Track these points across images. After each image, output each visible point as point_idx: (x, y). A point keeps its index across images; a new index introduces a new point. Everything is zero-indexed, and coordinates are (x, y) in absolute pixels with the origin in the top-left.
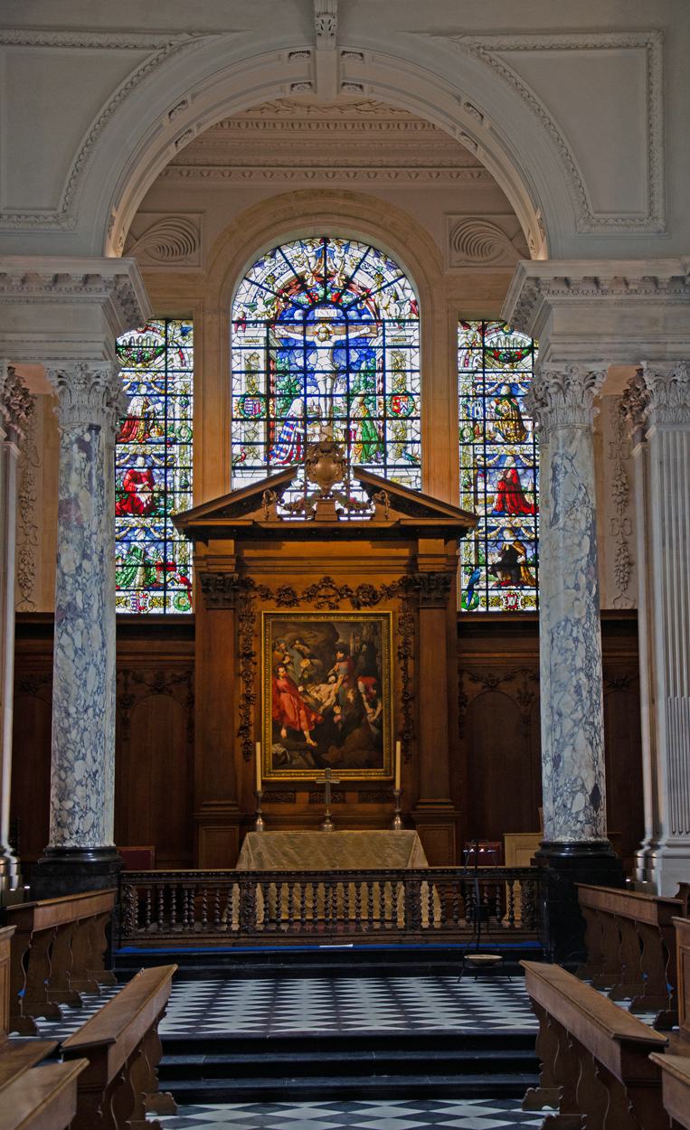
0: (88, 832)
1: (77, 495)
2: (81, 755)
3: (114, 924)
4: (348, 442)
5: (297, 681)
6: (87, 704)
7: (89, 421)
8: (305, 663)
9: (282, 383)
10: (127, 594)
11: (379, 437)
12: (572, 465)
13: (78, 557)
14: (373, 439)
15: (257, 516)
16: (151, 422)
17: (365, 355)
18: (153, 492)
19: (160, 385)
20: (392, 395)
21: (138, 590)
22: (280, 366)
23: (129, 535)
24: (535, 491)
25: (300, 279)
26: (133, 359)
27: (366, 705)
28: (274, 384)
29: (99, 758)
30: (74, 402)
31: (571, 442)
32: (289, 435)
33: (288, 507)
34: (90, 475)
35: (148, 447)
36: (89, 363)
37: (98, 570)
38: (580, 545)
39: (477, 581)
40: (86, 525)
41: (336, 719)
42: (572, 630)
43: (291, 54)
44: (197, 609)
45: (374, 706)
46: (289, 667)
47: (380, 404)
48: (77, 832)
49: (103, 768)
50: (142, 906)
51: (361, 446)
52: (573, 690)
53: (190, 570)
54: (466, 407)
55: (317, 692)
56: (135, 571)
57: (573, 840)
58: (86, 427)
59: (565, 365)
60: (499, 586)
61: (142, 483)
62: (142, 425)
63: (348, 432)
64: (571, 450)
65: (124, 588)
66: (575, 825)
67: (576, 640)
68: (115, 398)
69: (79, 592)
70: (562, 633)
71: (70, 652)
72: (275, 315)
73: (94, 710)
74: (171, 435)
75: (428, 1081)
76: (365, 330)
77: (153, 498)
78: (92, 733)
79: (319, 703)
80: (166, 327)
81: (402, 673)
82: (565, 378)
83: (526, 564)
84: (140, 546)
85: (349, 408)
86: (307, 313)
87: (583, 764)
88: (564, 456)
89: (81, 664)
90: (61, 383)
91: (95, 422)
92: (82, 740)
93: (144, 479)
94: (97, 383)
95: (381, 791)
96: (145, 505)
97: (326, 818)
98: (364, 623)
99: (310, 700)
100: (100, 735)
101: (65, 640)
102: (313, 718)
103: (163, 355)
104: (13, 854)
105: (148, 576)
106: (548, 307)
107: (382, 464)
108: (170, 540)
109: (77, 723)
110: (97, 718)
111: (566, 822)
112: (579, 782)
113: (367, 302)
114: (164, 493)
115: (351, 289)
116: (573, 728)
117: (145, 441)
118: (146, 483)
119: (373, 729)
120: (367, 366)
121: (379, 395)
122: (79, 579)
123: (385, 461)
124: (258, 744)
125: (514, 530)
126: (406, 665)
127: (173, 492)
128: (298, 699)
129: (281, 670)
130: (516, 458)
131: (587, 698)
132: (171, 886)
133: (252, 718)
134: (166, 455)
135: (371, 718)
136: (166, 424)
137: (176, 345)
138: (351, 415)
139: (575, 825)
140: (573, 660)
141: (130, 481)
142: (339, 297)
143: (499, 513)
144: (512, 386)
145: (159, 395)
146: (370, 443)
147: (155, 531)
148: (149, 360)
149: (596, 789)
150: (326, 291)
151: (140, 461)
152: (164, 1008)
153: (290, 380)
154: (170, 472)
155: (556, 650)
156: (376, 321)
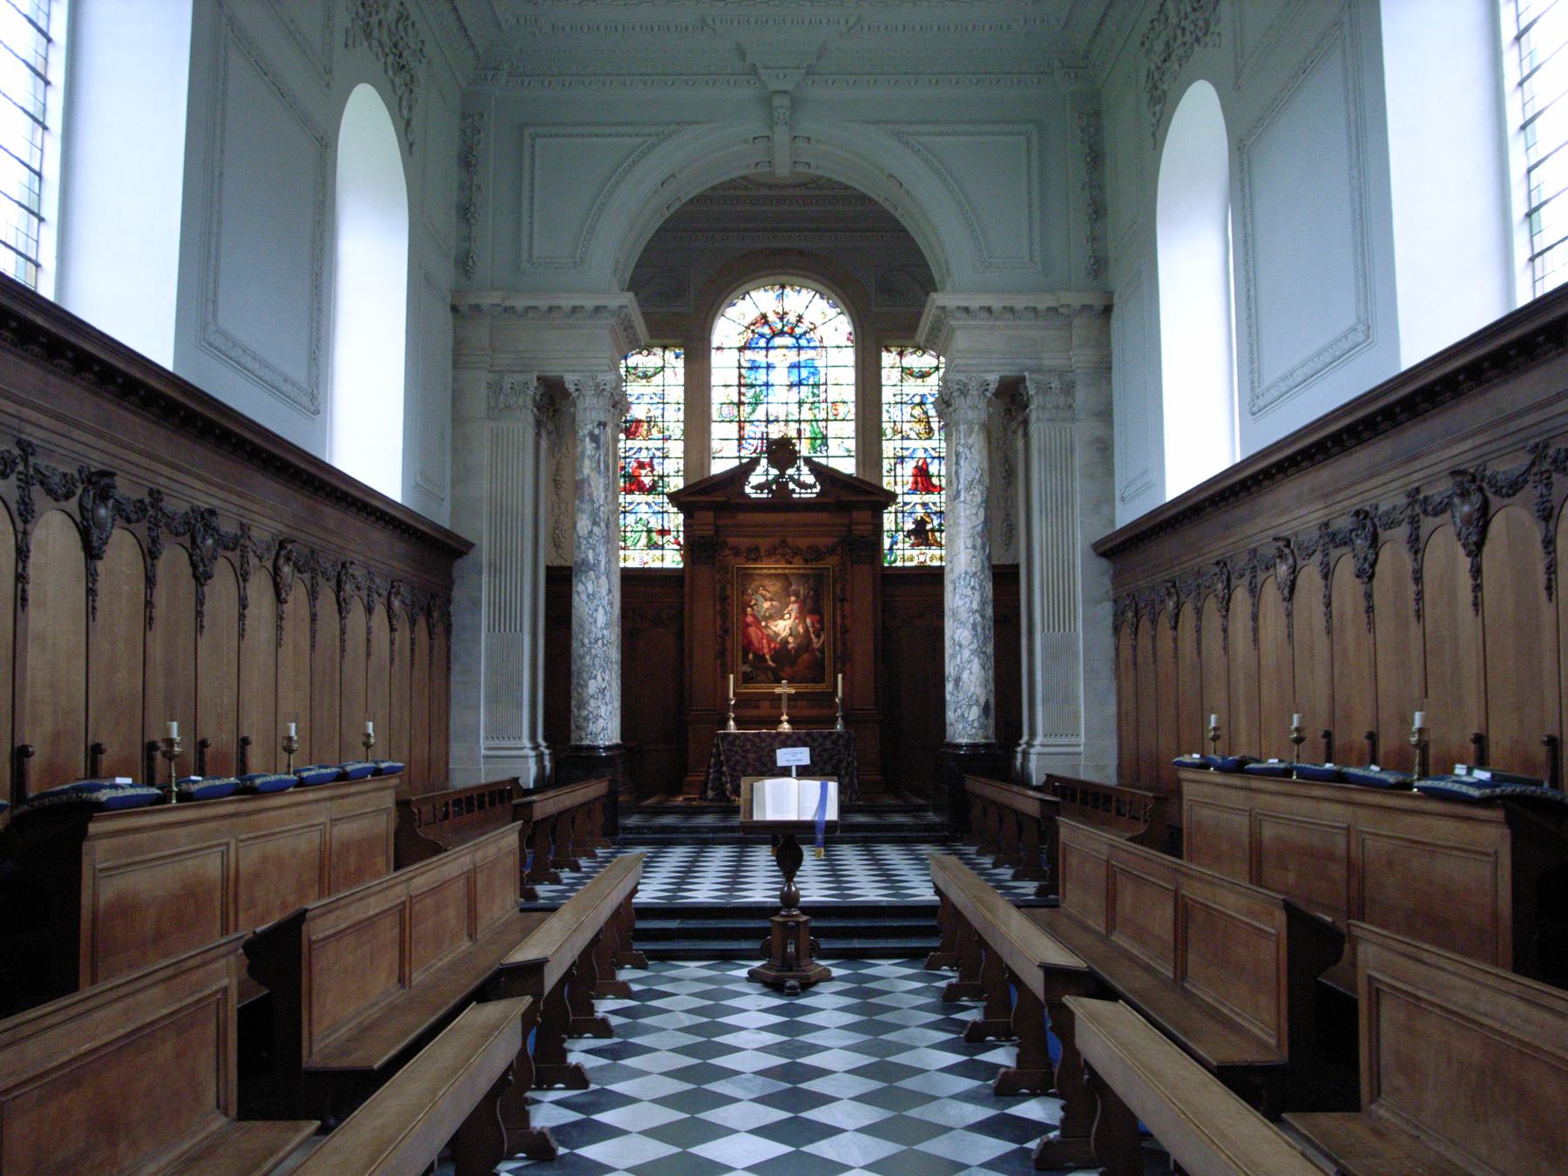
1: (588, 476)
3: (610, 806)
4: (799, 438)
5: (760, 617)
7: (598, 419)
9: (750, 393)
13: (589, 523)
20: (833, 403)
24: (939, 476)
26: (639, 377)
27: (813, 636)
29: (607, 678)
30: (587, 405)
33: (753, 488)
34: (599, 459)
36: (598, 374)
37: (605, 534)
39: (896, 543)
40: (595, 499)
41: (790, 646)
43: (755, 138)
44: (685, 564)
45: (818, 636)
46: (755, 607)
49: (610, 686)
51: (809, 441)
53: (681, 534)
54: (888, 411)
57: (969, 741)
58: (595, 424)
60: (913, 546)
62: (646, 425)
63: (799, 431)
64: (971, 441)
68: (620, 403)
69: (591, 551)
70: (962, 583)
71: (584, 597)
74: (667, 433)
75: (857, 944)
76: (811, 354)
79: (777, 635)
82: (965, 385)
83: (933, 530)
84: (645, 517)
86: (768, 341)
88: (965, 445)
89: (592, 606)
90: (577, 390)
91: (603, 420)
92: (594, 664)
94: (604, 390)
99: (771, 632)
101: (580, 588)
102: (773, 645)
104: (547, 747)
105: (650, 539)
106: (953, 330)
107: (825, 454)
108: (666, 512)
111: (964, 728)
112: (974, 697)
114: (662, 477)
117: (648, 438)
119: (818, 654)
125: (924, 505)
127: (668, 476)
129: (749, 609)
130: (926, 450)
134: (663, 449)
135: (816, 646)
140: (971, 603)
143: (914, 490)
144: (923, 396)
146: (815, 439)
148: (651, 377)
149: (987, 702)
151: (644, 453)
152: (636, 887)
154: (666, 461)
155: (958, 596)
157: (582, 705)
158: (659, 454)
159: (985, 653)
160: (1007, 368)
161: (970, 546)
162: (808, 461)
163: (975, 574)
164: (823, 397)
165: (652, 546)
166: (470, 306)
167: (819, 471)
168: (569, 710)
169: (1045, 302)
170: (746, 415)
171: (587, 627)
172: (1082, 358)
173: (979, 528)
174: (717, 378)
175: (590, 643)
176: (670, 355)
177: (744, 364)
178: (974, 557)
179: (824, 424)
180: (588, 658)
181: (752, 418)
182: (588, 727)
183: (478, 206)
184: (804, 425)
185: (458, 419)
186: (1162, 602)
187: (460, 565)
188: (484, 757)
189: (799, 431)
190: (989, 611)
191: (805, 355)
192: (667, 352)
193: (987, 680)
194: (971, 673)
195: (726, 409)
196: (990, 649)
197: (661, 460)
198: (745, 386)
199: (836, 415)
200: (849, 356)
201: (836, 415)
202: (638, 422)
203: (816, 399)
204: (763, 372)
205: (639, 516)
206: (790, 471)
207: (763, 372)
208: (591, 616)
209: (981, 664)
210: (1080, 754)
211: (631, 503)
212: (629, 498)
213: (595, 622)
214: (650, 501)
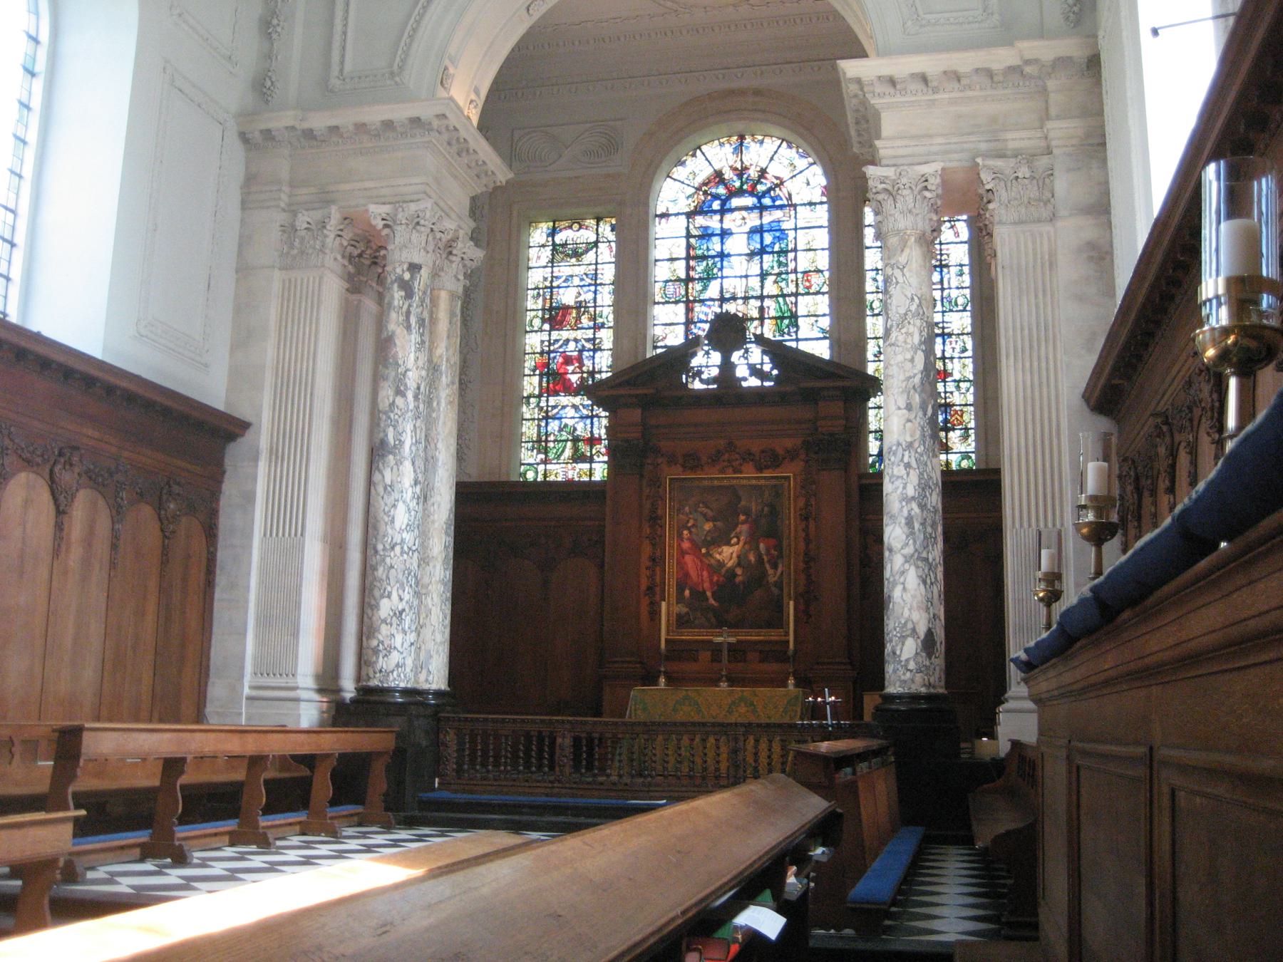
0: (392, 672)
2: (387, 593)
6: (394, 541)
7: (409, 260)
8: (708, 526)
9: (701, 267)
10: (558, 466)
11: (791, 312)
12: (904, 275)
13: (391, 393)
14: (786, 315)
16: (583, 309)
17: (778, 237)
18: (583, 372)
19: (590, 276)
20: (805, 273)
21: (567, 463)
22: (699, 252)
23: (561, 412)
25: (719, 175)
27: (768, 566)
28: (693, 269)
29: (406, 597)
31: (902, 251)
32: (706, 315)
35: (579, 332)
38: (912, 360)
40: (400, 362)
42: (903, 455)
45: (775, 567)
47: (792, 281)
48: (381, 671)
50: (460, 750)
51: (774, 322)
52: (903, 521)
54: (875, 280)
55: (720, 554)
56: (565, 446)
58: (405, 266)
59: (893, 169)
61: (573, 365)
63: (761, 309)
65: (555, 461)
66: (904, 674)
67: (908, 466)
69: (391, 429)
72: (696, 207)
73: (402, 548)
74: (599, 320)
76: (778, 214)
77: (582, 377)
78: (399, 571)
79: (721, 564)
80: (598, 225)
81: (804, 535)
82: (894, 183)
84: (570, 422)
85: (762, 287)
86: (724, 203)
87: (915, 605)
92: (388, 578)
93: (574, 361)
95: (775, 653)
96: (575, 385)
97: (722, 676)
98: (765, 486)
99: (713, 561)
100: (409, 574)
102: (715, 578)
103: (595, 249)
105: (576, 449)
109: (384, 560)
110: (405, 556)
112: (910, 626)
113: (780, 189)
115: (766, 178)
116: (903, 565)
118: (577, 365)
119: (775, 591)
120: (780, 247)
121: (791, 272)
122: (392, 415)
123: (797, 335)
124: (664, 605)
126: (807, 527)
128: (701, 561)
129: (685, 532)
131: (919, 530)
132: (532, 733)
133: (658, 580)
134: (594, 339)
136: (595, 311)
137: (605, 240)
138: (765, 293)
139: (904, 674)
140: (904, 488)
141: (562, 364)
142: (754, 187)
145: (590, 285)
146: (782, 318)
147: (584, 408)
148: (582, 254)
149: (930, 633)
150: (742, 182)
151: (572, 345)
153: (708, 264)
154: (598, 354)
156: (789, 205)
158: (589, 346)
159: (926, 560)
160: (956, 156)
161: (902, 405)
162: (760, 340)
163: (910, 445)
164: (791, 266)
165: (578, 458)
166: (261, 131)
169: (1002, 58)
170: (695, 294)
171: (382, 528)
173: (917, 380)
174: (660, 250)
175: (384, 549)
177: (694, 232)
178: (909, 421)
179: (793, 299)
180: (381, 569)
181: (704, 296)
182: (376, 662)
183: (282, 18)
184: (767, 303)
187: (235, 453)
188: (250, 698)
189: (761, 309)
191: (768, 218)
192: (601, 224)
193: (930, 601)
194: (904, 589)
195: (671, 288)
196: (936, 553)
197: (591, 353)
198: (696, 258)
199: (808, 288)
200: (822, 215)
201: (808, 288)
202: (566, 309)
203: (783, 269)
204: (716, 240)
205: (564, 421)
207: (716, 240)
208: (387, 514)
209: (920, 577)
211: (554, 407)
212: (552, 401)
213: (393, 521)
214: (578, 404)
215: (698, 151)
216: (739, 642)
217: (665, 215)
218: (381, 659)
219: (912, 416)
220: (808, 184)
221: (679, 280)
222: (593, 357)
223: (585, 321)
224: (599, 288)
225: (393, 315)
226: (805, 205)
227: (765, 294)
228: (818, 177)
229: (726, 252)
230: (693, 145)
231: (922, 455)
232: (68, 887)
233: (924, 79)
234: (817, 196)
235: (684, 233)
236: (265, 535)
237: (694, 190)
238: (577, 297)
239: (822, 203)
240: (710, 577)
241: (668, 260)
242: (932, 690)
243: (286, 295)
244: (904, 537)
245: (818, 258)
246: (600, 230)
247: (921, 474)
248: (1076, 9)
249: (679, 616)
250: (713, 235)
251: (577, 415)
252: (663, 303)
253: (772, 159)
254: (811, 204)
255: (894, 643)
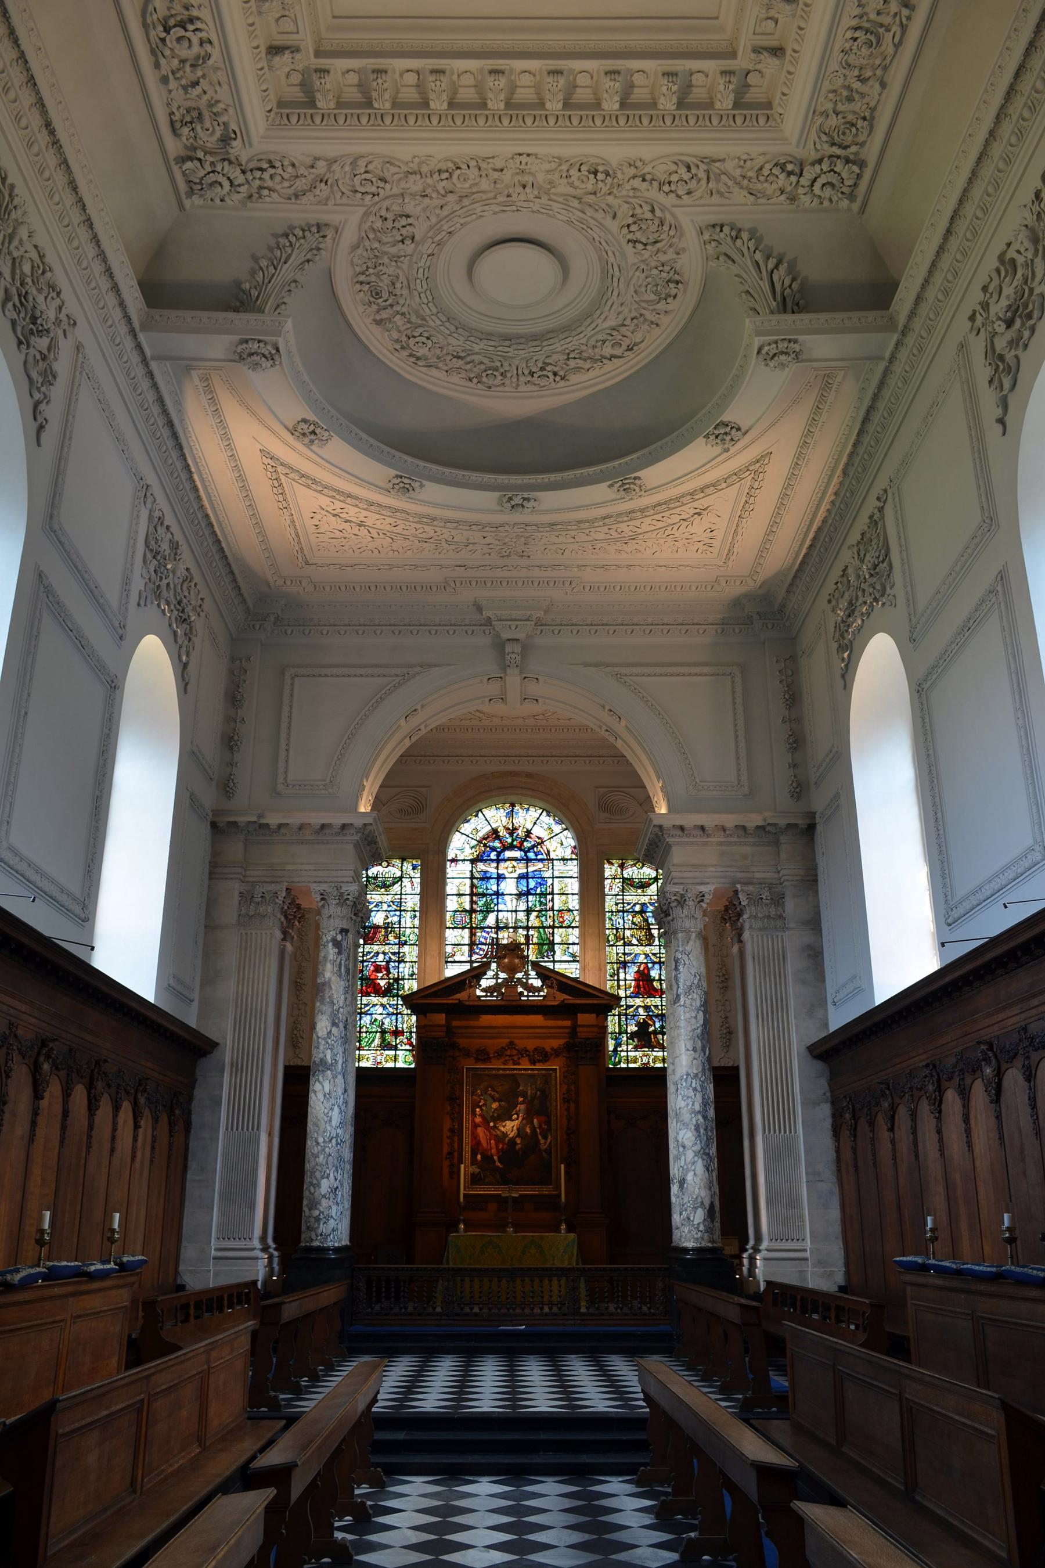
4: (527, 944)
8: (495, 1105)
10: (369, 1052)
13: (328, 1024)
15: (462, 996)
18: (389, 979)
20: (559, 911)
22: (480, 891)
25: (495, 832)
27: (540, 1137)
28: (476, 903)
32: (486, 939)
35: (387, 947)
40: (335, 1001)
45: (545, 1138)
48: (321, 1235)
55: (504, 1127)
63: (527, 937)
67: (695, 1089)
68: (360, 910)
71: (321, 1096)
72: (478, 855)
76: (540, 865)
77: (389, 982)
79: (505, 1135)
80: (402, 864)
82: (682, 896)
84: (379, 1018)
85: (528, 920)
86: (499, 854)
92: (327, 1163)
99: (498, 1132)
102: (501, 1146)
105: (383, 1039)
109: (324, 1150)
112: (699, 1200)
114: (397, 980)
115: (530, 838)
124: (462, 1166)
128: (490, 1132)
129: (478, 1110)
130: (647, 956)
134: (399, 953)
140: (693, 1105)
142: (522, 843)
143: (636, 995)
145: (396, 910)
146: (543, 944)
148: (390, 886)
149: (712, 1205)
151: (381, 957)
154: (402, 965)
156: (547, 859)
157: (314, 1204)
162: (536, 965)
163: (696, 1075)
165: (385, 1046)
167: (545, 974)
168: (300, 1210)
172: (790, 870)
173: (699, 1031)
174: (451, 888)
176: (408, 867)
177: (477, 875)
178: (695, 1059)
179: (551, 931)
182: (318, 1227)
184: (531, 932)
185: (211, 926)
186: (877, 1104)
188: (215, 1258)
190: (711, 1113)
193: (711, 1182)
197: (397, 964)
198: (477, 895)
199: (562, 922)
200: (573, 868)
201: (562, 922)
206: (519, 975)
209: (705, 1166)
210: (806, 1259)
211: (367, 1005)
215: (480, 813)
216: (521, 1195)
217: (454, 860)
218: (321, 1225)
219: (697, 1056)
220: (562, 844)
221: (465, 911)
222: (398, 968)
223: (391, 938)
224: (403, 913)
225: (329, 966)
226: (559, 860)
227: (530, 925)
228: (569, 840)
229: (500, 892)
230: (477, 809)
231: (703, 1082)
232: (19, 1416)
233: (703, 828)
234: (568, 854)
235: (468, 875)
236: (227, 1129)
237: (476, 843)
238: (385, 920)
239: (571, 859)
240: (497, 1145)
241: (456, 895)
242: (715, 1245)
243: (244, 945)
244: (694, 1138)
245: (570, 900)
246: (404, 868)
247: (704, 1095)
248: (798, 790)
249: (473, 1175)
250: (490, 878)
251: (384, 1012)
252: (453, 928)
253: (535, 823)
254: (563, 859)
255: (688, 1212)
